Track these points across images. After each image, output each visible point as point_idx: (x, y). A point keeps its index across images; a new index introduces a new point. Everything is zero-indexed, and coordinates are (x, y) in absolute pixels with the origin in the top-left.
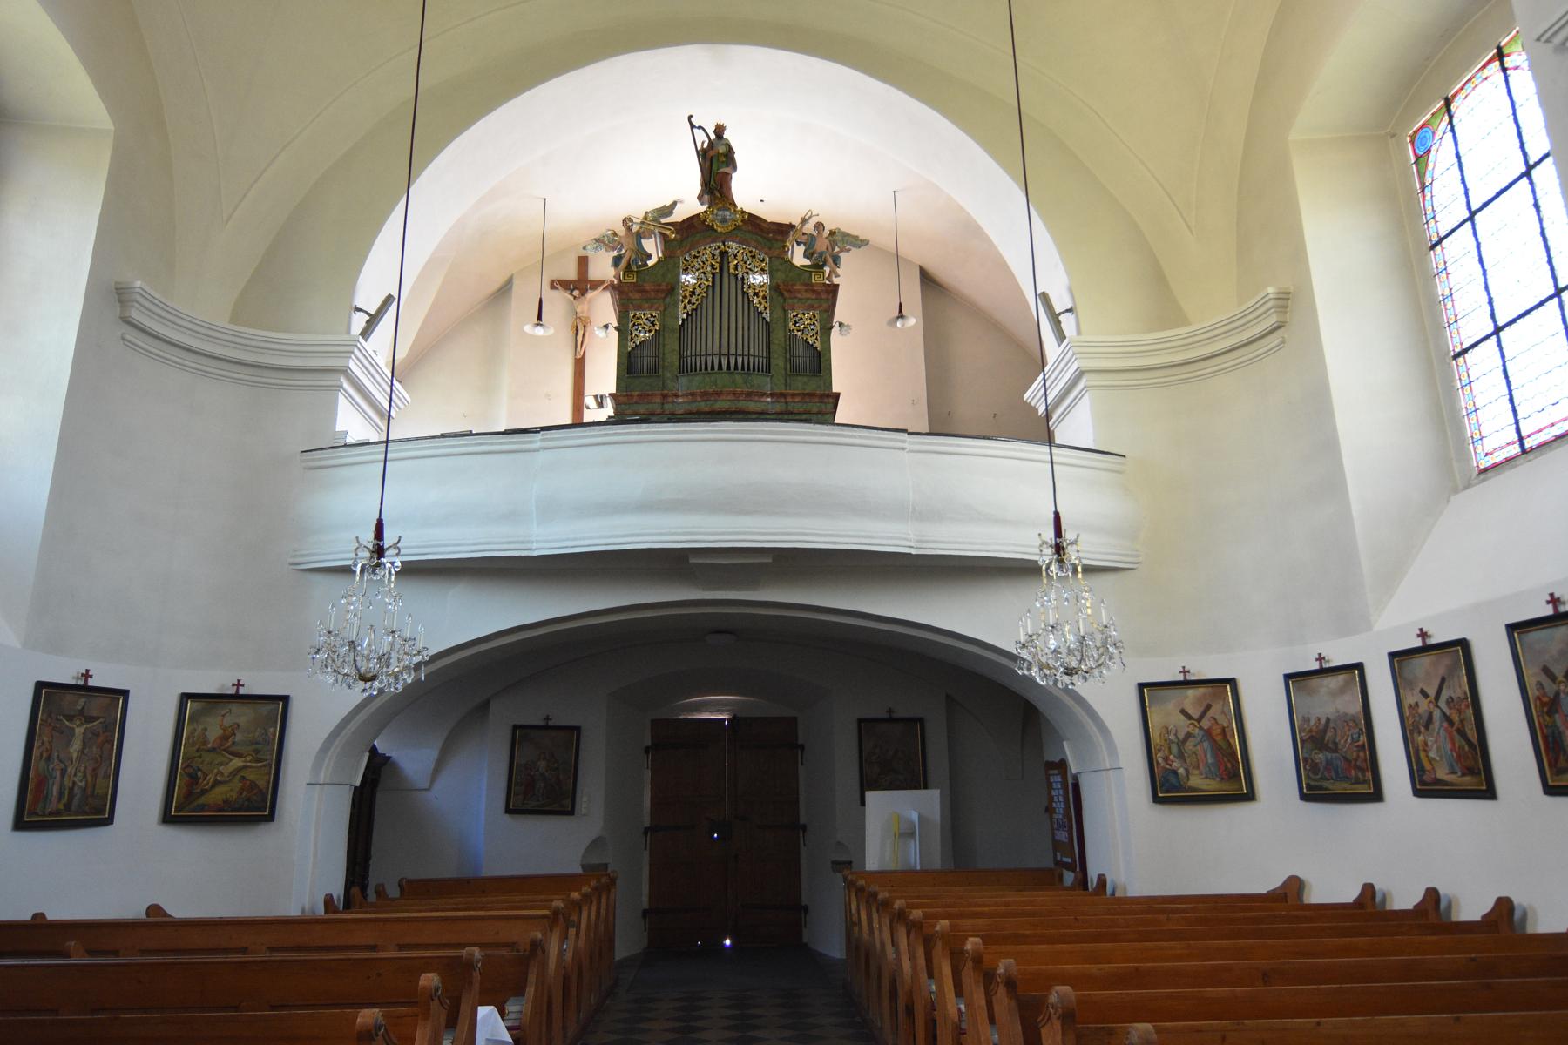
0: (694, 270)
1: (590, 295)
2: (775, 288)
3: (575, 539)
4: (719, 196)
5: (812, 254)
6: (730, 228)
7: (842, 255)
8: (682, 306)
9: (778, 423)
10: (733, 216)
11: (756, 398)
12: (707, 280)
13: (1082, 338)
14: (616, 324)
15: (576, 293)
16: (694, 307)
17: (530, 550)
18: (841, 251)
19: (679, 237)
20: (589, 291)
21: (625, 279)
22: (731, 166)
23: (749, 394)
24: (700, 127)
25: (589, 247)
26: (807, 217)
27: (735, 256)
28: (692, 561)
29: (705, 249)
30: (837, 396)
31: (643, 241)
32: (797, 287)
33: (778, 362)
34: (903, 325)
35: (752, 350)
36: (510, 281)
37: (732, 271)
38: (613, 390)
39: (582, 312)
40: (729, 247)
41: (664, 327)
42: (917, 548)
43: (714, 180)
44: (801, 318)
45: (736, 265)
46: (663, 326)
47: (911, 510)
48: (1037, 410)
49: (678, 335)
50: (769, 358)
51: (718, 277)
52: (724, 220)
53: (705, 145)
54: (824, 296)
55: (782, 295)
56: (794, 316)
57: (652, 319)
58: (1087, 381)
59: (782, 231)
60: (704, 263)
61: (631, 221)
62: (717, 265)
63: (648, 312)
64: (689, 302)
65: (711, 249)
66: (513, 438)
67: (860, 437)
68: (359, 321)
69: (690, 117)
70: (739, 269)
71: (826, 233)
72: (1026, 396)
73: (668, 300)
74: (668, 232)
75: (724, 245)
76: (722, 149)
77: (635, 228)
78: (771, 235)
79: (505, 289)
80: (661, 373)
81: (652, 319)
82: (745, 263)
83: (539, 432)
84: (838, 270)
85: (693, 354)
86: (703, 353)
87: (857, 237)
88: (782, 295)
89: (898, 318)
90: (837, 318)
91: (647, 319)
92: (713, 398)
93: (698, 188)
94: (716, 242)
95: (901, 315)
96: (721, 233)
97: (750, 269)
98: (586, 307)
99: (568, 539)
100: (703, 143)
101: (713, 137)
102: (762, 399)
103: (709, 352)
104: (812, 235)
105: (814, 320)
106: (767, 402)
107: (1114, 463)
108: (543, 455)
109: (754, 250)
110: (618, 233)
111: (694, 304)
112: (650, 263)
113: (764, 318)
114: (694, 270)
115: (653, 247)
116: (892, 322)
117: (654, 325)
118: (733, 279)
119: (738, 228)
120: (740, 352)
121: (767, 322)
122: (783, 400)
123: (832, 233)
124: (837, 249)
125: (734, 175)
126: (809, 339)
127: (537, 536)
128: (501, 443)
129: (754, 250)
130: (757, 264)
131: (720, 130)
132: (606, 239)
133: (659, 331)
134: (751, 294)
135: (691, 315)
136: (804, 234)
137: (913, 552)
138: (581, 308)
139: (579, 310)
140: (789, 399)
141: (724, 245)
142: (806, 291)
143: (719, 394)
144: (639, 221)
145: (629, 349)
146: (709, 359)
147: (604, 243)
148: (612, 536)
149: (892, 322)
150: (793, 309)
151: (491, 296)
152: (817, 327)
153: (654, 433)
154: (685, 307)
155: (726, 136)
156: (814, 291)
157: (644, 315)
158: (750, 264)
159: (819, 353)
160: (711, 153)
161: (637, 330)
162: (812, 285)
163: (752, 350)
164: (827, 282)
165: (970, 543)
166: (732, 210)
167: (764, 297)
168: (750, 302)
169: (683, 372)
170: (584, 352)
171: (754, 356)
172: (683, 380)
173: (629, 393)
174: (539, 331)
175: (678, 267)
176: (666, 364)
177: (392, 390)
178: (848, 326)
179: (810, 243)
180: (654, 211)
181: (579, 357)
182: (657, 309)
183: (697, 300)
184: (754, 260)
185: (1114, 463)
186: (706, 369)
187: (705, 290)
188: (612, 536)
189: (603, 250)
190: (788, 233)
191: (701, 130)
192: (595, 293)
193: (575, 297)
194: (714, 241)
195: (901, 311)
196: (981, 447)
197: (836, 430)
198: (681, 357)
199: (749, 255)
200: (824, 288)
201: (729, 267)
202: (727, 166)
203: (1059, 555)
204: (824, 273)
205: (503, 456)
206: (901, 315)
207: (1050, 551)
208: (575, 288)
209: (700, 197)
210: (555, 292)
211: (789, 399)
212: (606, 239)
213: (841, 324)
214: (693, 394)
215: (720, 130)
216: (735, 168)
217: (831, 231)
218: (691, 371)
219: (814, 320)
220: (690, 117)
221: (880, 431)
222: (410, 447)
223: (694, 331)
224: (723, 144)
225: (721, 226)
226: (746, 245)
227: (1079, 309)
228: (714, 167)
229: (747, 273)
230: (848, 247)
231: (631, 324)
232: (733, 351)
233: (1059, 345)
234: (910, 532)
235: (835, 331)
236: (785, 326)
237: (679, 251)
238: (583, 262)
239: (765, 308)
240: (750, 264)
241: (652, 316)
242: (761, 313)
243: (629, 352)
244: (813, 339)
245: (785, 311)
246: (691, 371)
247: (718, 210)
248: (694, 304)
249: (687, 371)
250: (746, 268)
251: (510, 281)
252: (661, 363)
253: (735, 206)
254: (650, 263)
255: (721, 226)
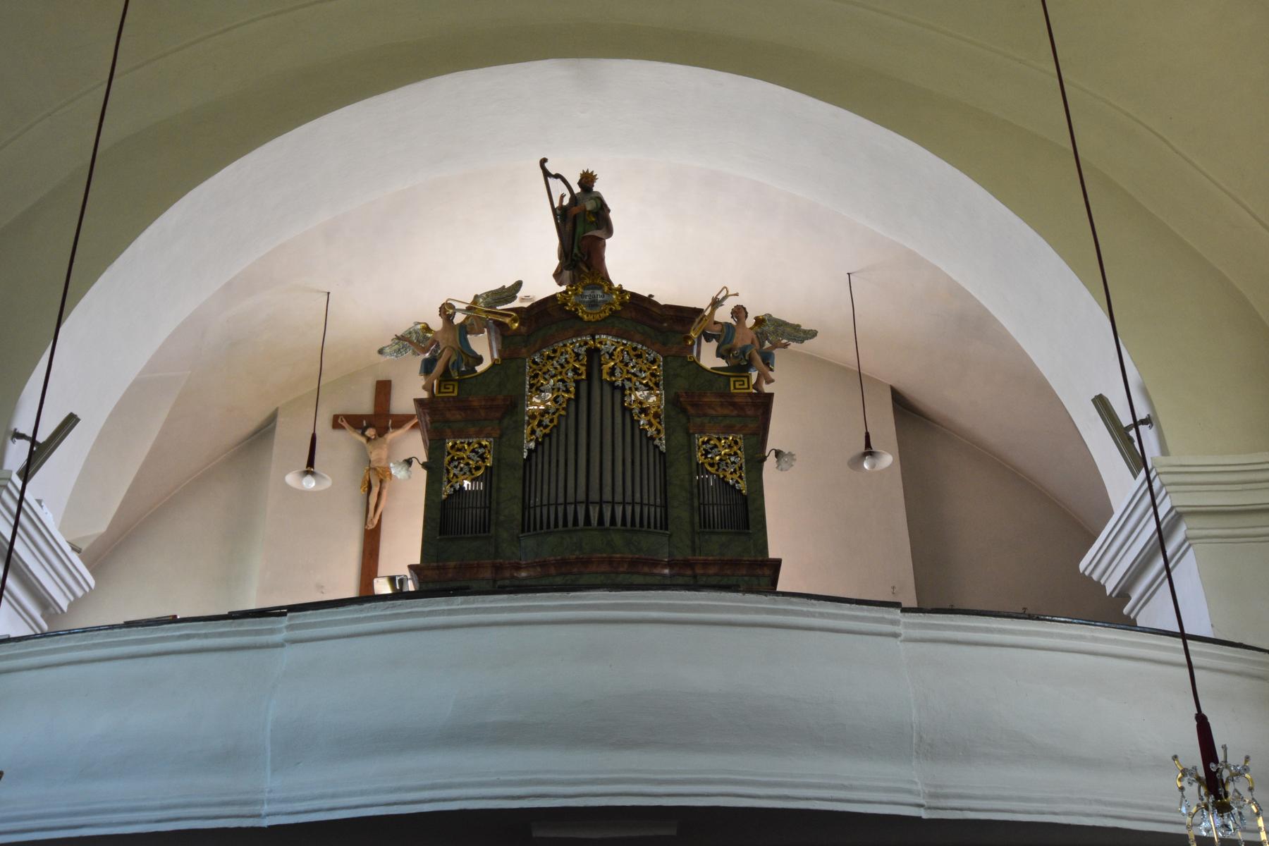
0: (547, 376)
1: (392, 435)
2: (674, 402)
3: (334, 796)
4: (586, 270)
5: (730, 351)
6: (603, 315)
7: (776, 352)
8: (527, 430)
9: (683, 592)
10: (606, 297)
11: (646, 569)
12: (567, 391)
13: (1172, 459)
14: (424, 458)
15: (371, 432)
16: (547, 431)
17: (259, 816)
18: (775, 346)
19: (524, 329)
20: (391, 430)
21: (439, 392)
22: (604, 229)
23: (634, 563)
24: (557, 176)
25: (387, 350)
26: (720, 297)
27: (611, 355)
28: (537, 833)
29: (565, 345)
30: (777, 564)
31: (468, 336)
32: (709, 398)
33: (680, 512)
34: (873, 466)
35: (638, 495)
36: (272, 419)
37: (605, 376)
38: (417, 560)
39: (380, 460)
40: (601, 343)
41: (499, 461)
42: (930, 808)
43: (579, 249)
44: (715, 446)
45: (613, 369)
46: (497, 460)
47: (915, 740)
48: (1104, 587)
49: (521, 472)
50: (665, 506)
51: (584, 386)
52: (593, 304)
53: (566, 202)
54: (750, 412)
55: (684, 411)
56: (704, 443)
57: (481, 451)
58: (1188, 529)
59: (684, 317)
60: (562, 366)
61: (452, 307)
62: (583, 369)
63: (475, 440)
64: (540, 424)
65: (574, 346)
66: (240, 625)
67: (822, 615)
68: (17, 454)
69: (543, 161)
70: (617, 372)
71: (750, 322)
72: (1082, 566)
73: (506, 422)
74: (507, 320)
75: (594, 339)
76: (590, 205)
77: (459, 318)
78: (665, 325)
79: (264, 432)
80: (493, 531)
81: (481, 451)
82: (627, 365)
83: (284, 614)
84: (770, 373)
85: (545, 502)
86: (561, 500)
87: (799, 326)
88: (684, 411)
89: (865, 454)
90: (772, 443)
91: (473, 451)
92: (575, 570)
93: (555, 262)
94: (580, 336)
95: (869, 452)
96: (589, 322)
97: (634, 374)
98: (384, 453)
99: (322, 797)
100: (562, 197)
101: (577, 190)
102: (656, 571)
103: (571, 499)
104: (728, 325)
105: (735, 448)
106: (664, 576)
107: (1254, 662)
108: (290, 652)
109: (640, 346)
110: (431, 326)
111: (546, 427)
112: (480, 369)
113: (656, 447)
114: (547, 376)
115: (483, 346)
116: (856, 462)
117: (483, 458)
118: (607, 389)
119: (614, 314)
120: (619, 498)
121: (661, 452)
122: (689, 572)
123: (759, 321)
124: (767, 344)
125: (608, 241)
126: (729, 477)
127: (271, 791)
128: (221, 635)
129: (640, 346)
130: (644, 367)
131: (587, 180)
132: (414, 337)
133: (491, 468)
134: (637, 411)
135: (542, 443)
136: (716, 323)
137: (925, 814)
138: (378, 454)
139: (373, 457)
140: (699, 571)
141: (594, 339)
142: (722, 405)
143: (586, 562)
144: (464, 307)
145: (444, 496)
146: (571, 509)
147: (411, 342)
148: (398, 790)
149: (856, 462)
150: (702, 433)
151: (239, 443)
152: (741, 460)
153: (476, 611)
154: (533, 432)
155: (597, 187)
156: (734, 405)
157: (469, 444)
158: (633, 367)
159: (745, 498)
160: (575, 210)
161: (456, 467)
162: (733, 395)
163: (638, 495)
164: (754, 391)
165: (1020, 799)
166: (606, 289)
167: (656, 415)
168: (634, 423)
169: (529, 531)
170: (380, 521)
171: (642, 504)
172: (529, 543)
173: (441, 564)
174: (310, 483)
175: (524, 374)
176: (502, 518)
177: (20, 508)
178: (791, 455)
179: (724, 337)
180: (488, 294)
181: (371, 527)
182: (487, 437)
183: (551, 421)
184: (640, 361)
185: (1254, 662)
186: (565, 524)
187: (564, 405)
188: (398, 790)
189: (410, 352)
190: (692, 321)
191: (559, 180)
192: (400, 432)
193: (369, 439)
194: (578, 334)
195: (868, 444)
196: (1027, 633)
197: (782, 604)
198: (525, 507)
199: (632, 353)
200: (750, 400)
201: (601, 371)
202: (598, 228)
203: (1217, 796)
204: (748, 378)
205: (224, 656)
206: (869, 452)
207: (1193, 790)
208: (369, 426)
209: (558, 276)
210: (339, 434)
211: (699, 571)
212: (414, 338)
213: (778, 454)
214: (544, 564)
215: (587, 180)
216: (609, 232)
217: (757, 319)
218: (541, 528)
219: (735, 448)
220: (543, 161)
221: (854, 606)
222: (72, 644)
223: (546, 466)
224: (592, 198)
225: (589, 311)
226: (628, 339)
227: (1162, 418)
228: (579, 229)
229: (629, 380)
230: (784, 341)
231: (447, 459)
232: (607, 496)
233: (1135, 477)
234: (916, 780)
235: (770, 465)
236: (690, 456)
237: (524, 350)
238: (383, 389)
239: (658, 431)
240: (633, 367)
241: (481, 446)
242: (652, 438)
243: (445, 500)
244: (736, 477)
245: (690, 436)
246: (541, 528)
247: (584, 288)
248: (546, 427)
249: (535, 529)
250: (628, 372)
251: (272, 419)
252: (493, 517)
253: (611, 283)
254: (480, 369)
255: (589, 311)
